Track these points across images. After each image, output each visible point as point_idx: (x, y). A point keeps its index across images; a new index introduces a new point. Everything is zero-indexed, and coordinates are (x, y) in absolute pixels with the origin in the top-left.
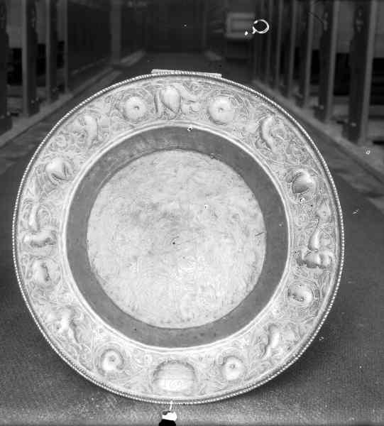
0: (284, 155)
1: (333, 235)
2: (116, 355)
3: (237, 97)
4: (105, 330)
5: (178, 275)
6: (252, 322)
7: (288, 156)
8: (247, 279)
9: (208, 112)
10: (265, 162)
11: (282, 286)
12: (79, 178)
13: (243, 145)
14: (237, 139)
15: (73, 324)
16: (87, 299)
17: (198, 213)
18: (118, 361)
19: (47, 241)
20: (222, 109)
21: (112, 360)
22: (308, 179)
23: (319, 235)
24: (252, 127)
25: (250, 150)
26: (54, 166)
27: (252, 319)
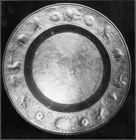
0: (113, 42)
1: (127, 76)
2: (42, 115)
3: (97, 17)
4: (38, 104)
5: (84, 95)
6: (43, 106)
7: (115, 43)
8: (94, 87)
9: (85, 21)
10: (105, 44)
11: (106, 93)
12: (30, 42)
13: (97, 35)
14: (95, 33)
15: (25, 101)
16: (31, 92)
17: (51, 17)
18: (42, 116)
19: (16, 68)
20: (90, 20)
21: (40, 115)
22: (121, 53)
23: (104, 110)
24: (102, 29)
25: (100, 38)
26: (21, 36)
27: (45, 106)
